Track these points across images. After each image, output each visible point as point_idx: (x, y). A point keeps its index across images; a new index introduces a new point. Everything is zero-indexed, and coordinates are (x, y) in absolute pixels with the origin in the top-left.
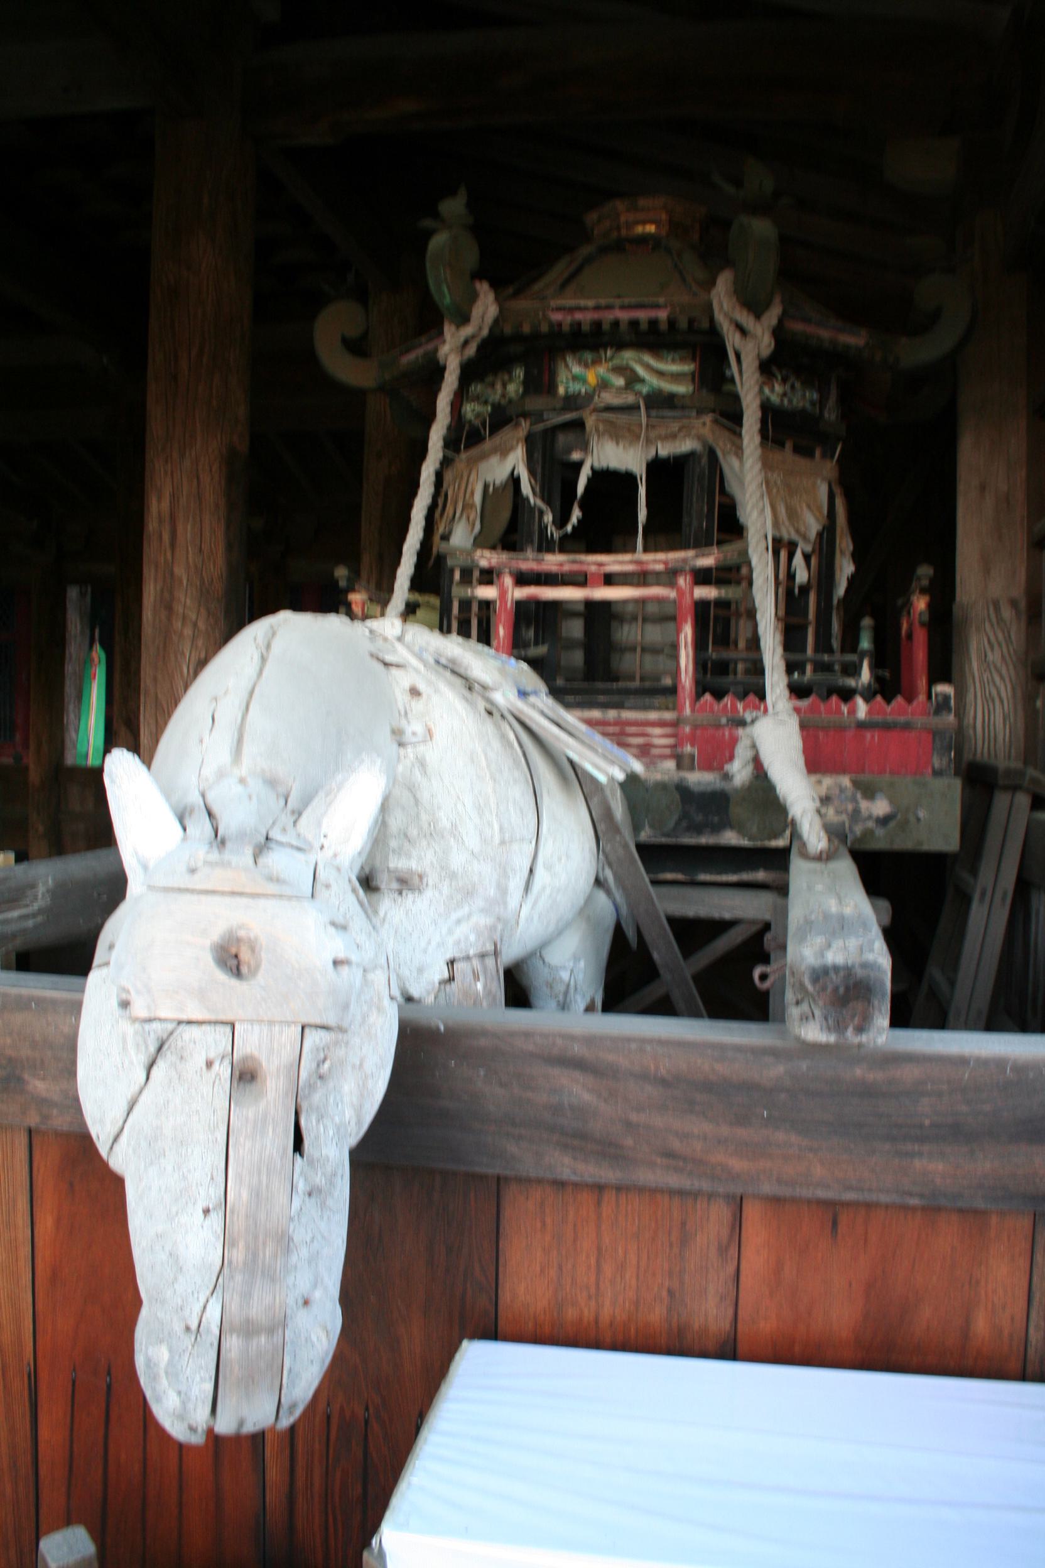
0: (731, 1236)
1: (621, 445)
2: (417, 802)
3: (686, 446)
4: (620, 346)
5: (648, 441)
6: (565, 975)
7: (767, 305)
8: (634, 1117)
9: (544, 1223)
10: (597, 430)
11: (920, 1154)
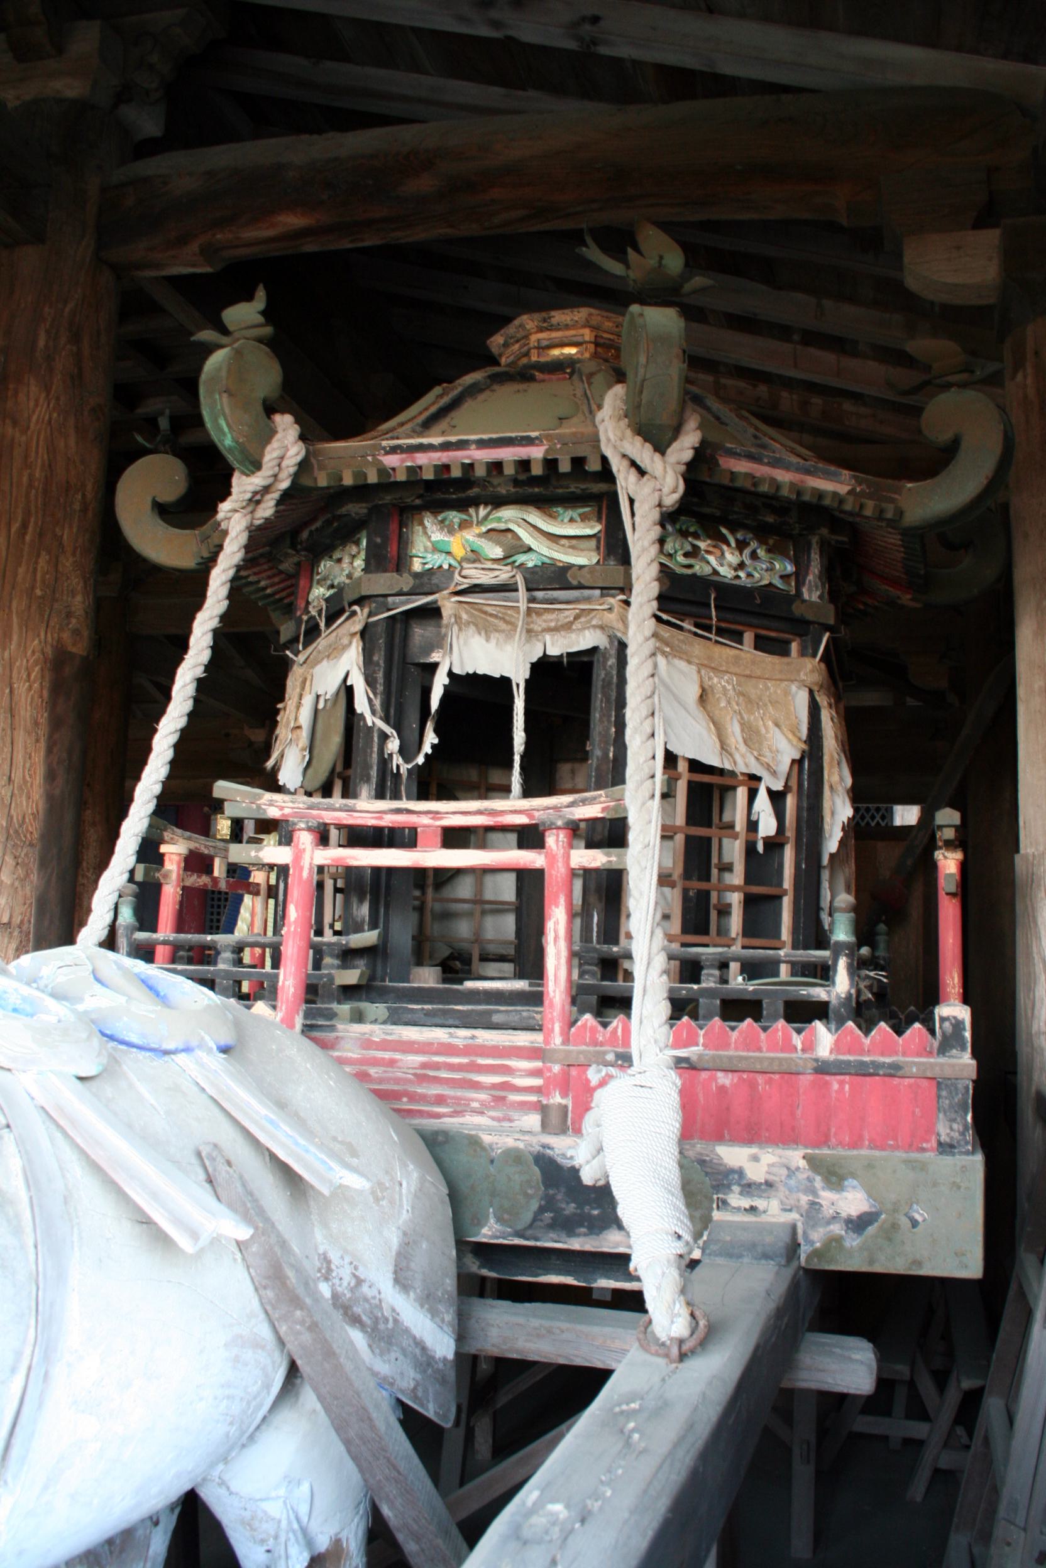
1: (493, 641)
3: (583, 640)
4: (498, 502)
6: (275, 1509)
7: (677, 431)
10: (457, 617)
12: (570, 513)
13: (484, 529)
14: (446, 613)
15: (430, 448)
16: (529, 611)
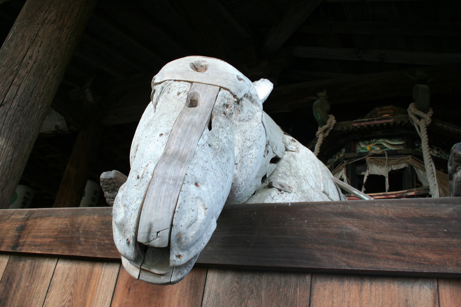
2: (290, 166)
3: (402, 166)
4: (378, 138)
8: (377, 236)
9: (333, 302)
12: (396, 140)
13: (374, 144)
14: (367, 160)
15: (365, 121)
16: (388, 159)
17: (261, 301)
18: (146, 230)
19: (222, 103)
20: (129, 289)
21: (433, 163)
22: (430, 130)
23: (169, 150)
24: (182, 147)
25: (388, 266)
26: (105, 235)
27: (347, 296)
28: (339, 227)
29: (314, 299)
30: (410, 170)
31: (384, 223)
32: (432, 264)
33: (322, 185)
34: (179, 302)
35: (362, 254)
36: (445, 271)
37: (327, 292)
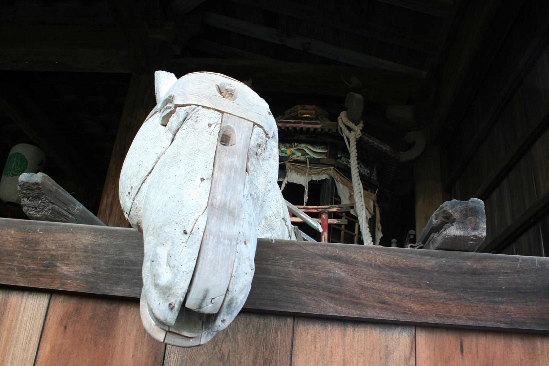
0: (411, 354)
3: (323, 177)
4: (300, 142)
5: (310, 175)
8: (365, 283)
9: (316, 347)
11: (503, 303)
12: (319, 147)
14: (287, 166)
15: (291, 123)
17: (238, 345)
18: (201, 296)
19: (257, 143)
20: (65, 327)
21: (360, 182)
22: (360, 144)
23: (215, 200)
24: (229, 198)
25: (375, 314)
26: (29, 258)
27: (330, 341)
28: (327, 271)
29: (297, 344)
30: (330, 183)
31: (372, 270)
32: (415, 313)
33: (282, 211)
34: (136, 344)
35: (350, 301)
36: (426, 321)
37: (309, 337)
